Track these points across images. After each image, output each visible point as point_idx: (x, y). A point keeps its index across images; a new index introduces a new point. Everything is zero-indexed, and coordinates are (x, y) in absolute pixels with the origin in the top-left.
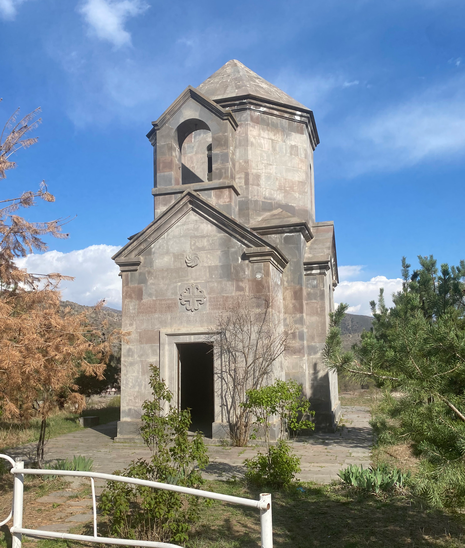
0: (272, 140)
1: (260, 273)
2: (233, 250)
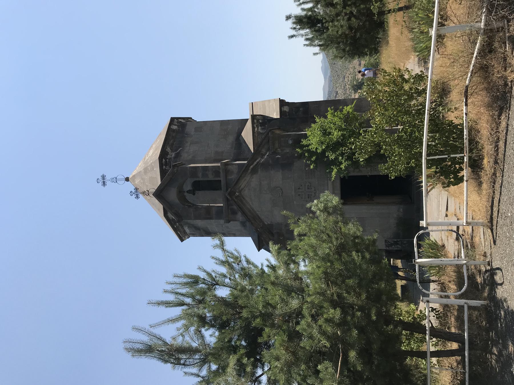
0: (190, 144)
1: (288, 141)
2: (270, 162)
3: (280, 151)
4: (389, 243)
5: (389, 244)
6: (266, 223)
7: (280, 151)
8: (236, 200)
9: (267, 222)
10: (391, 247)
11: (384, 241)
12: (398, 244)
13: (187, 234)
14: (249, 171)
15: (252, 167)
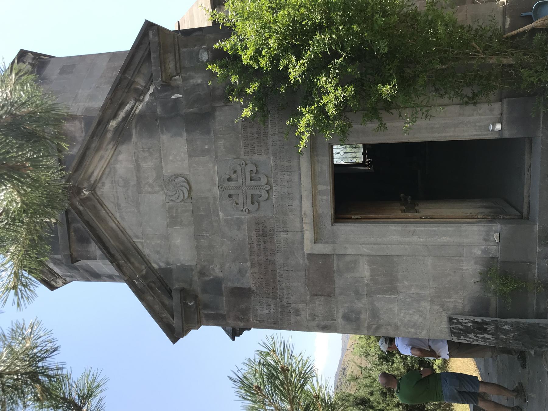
2: (159, 110)
3: (180, 82)
4: (461, 327)
5: (459, 329)
6: (155, 266)
7: (180, 82)
8: (81, 208)
9: (157, 263)
10: (466, 336)
11: (445, 319)
12: (485, 331)
13: (58, 275)
14: (109, 135)
15: (113, 124)
